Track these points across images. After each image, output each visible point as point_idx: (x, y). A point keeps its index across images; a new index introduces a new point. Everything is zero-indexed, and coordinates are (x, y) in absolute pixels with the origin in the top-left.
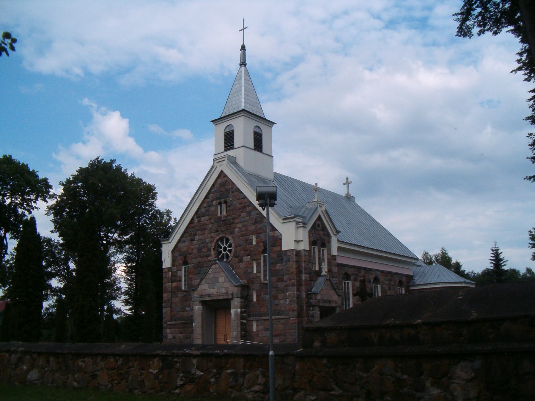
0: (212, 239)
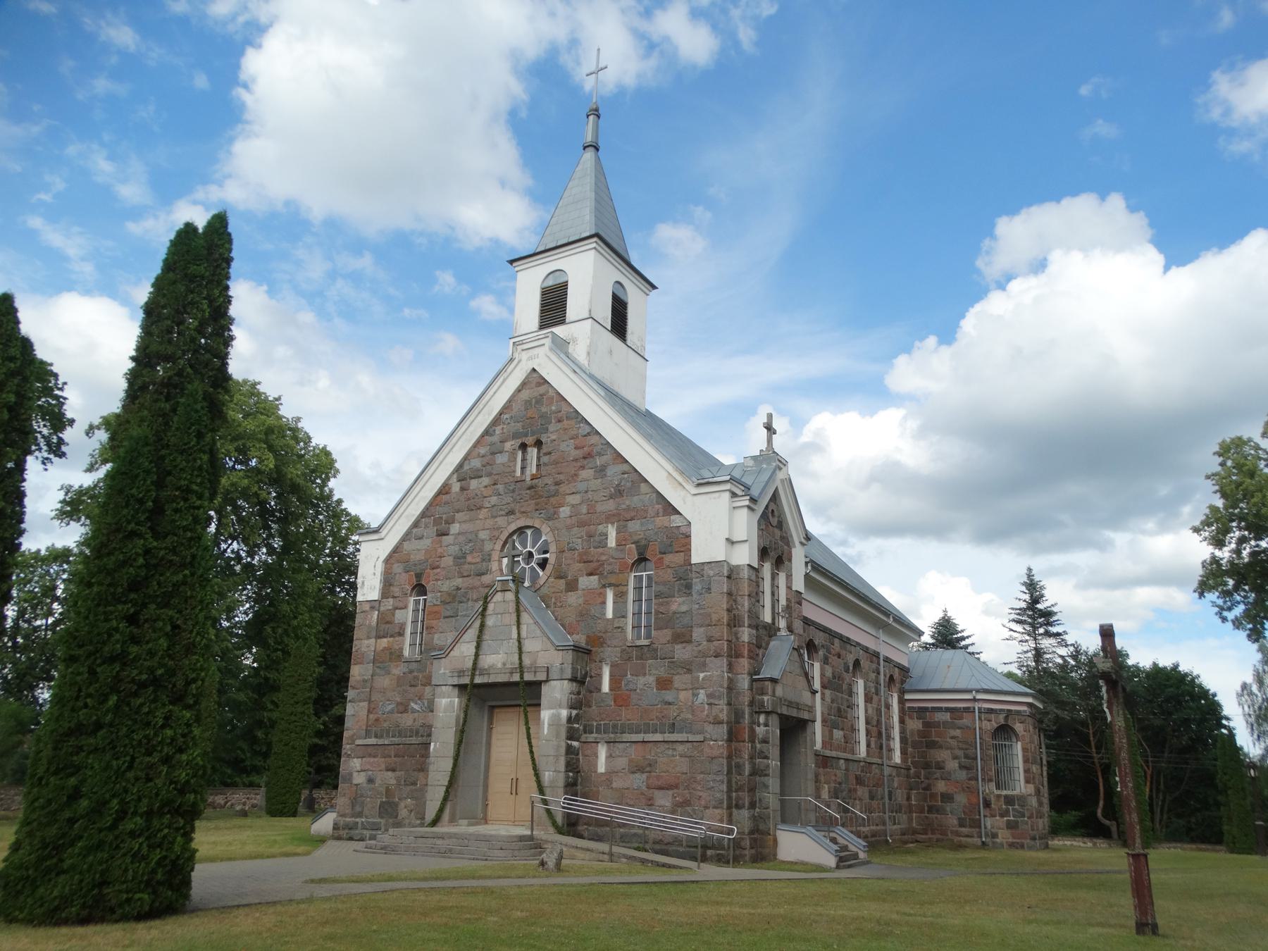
0: (496, 533)
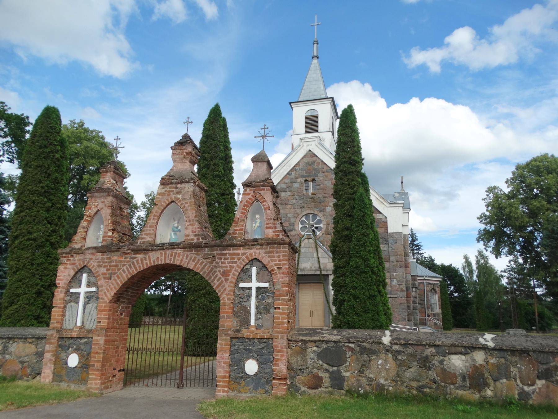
0: (296, 215)
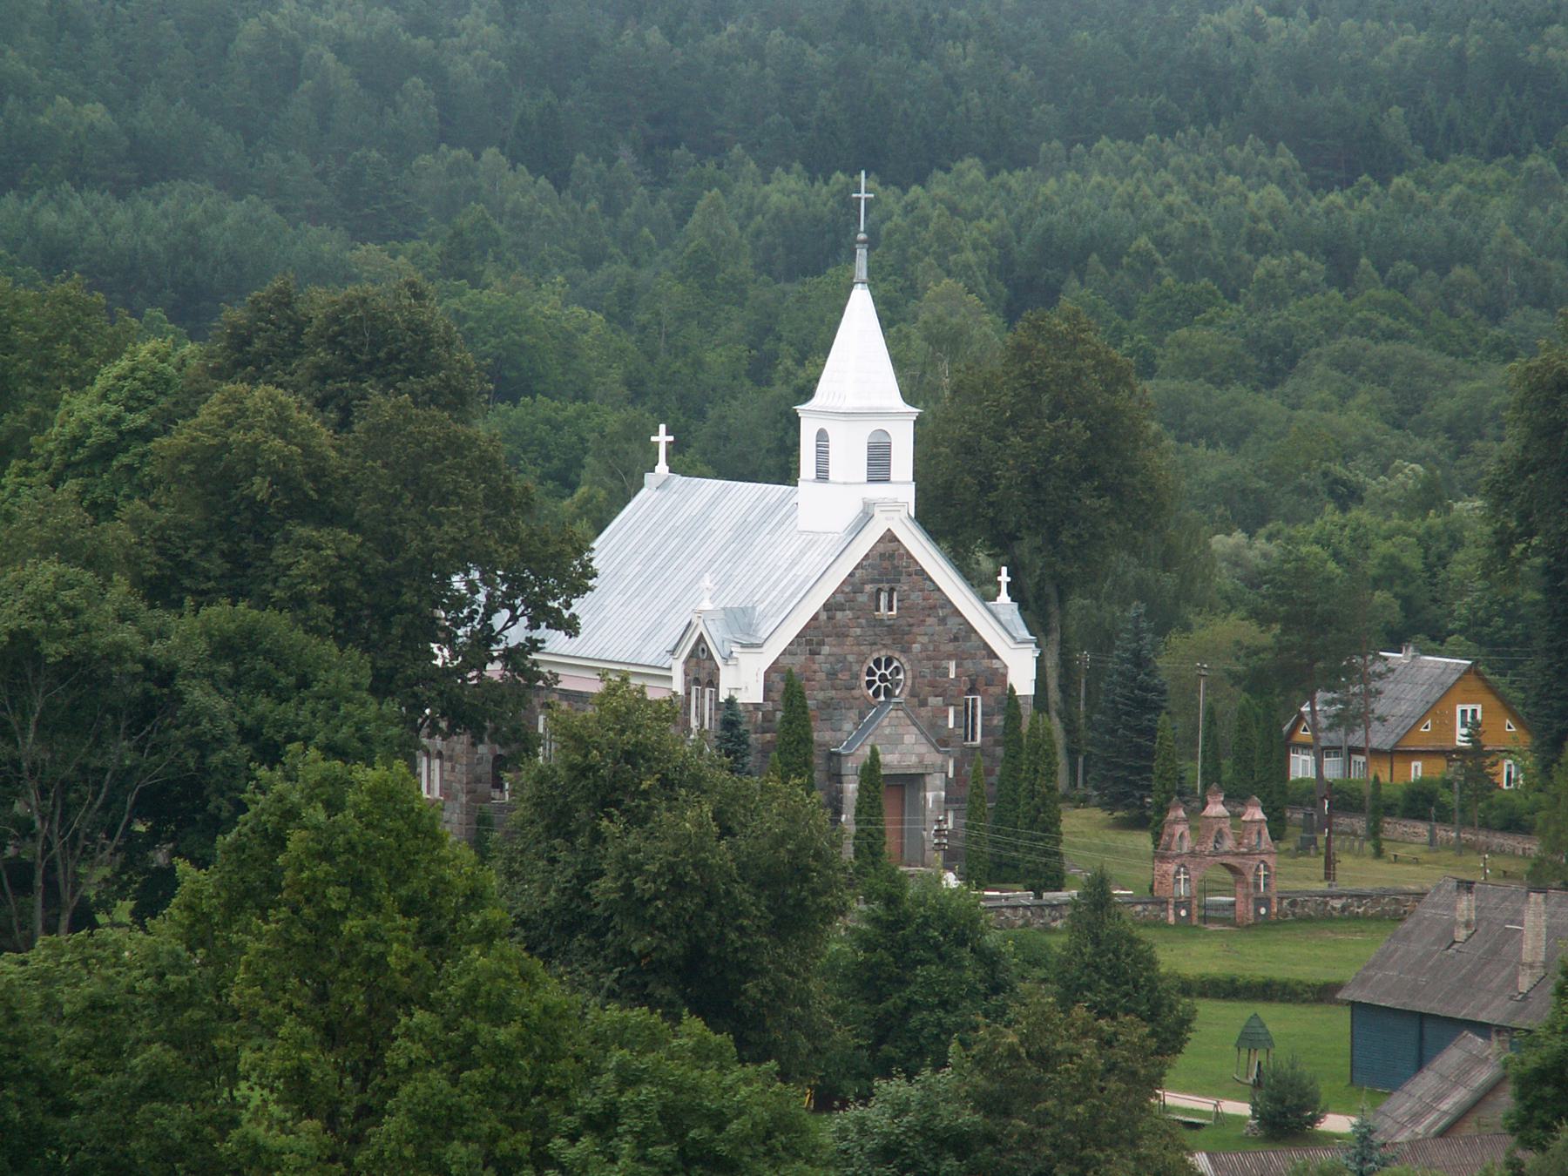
0: (862, 658)
